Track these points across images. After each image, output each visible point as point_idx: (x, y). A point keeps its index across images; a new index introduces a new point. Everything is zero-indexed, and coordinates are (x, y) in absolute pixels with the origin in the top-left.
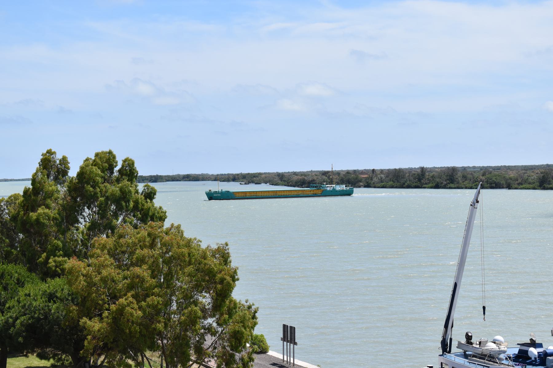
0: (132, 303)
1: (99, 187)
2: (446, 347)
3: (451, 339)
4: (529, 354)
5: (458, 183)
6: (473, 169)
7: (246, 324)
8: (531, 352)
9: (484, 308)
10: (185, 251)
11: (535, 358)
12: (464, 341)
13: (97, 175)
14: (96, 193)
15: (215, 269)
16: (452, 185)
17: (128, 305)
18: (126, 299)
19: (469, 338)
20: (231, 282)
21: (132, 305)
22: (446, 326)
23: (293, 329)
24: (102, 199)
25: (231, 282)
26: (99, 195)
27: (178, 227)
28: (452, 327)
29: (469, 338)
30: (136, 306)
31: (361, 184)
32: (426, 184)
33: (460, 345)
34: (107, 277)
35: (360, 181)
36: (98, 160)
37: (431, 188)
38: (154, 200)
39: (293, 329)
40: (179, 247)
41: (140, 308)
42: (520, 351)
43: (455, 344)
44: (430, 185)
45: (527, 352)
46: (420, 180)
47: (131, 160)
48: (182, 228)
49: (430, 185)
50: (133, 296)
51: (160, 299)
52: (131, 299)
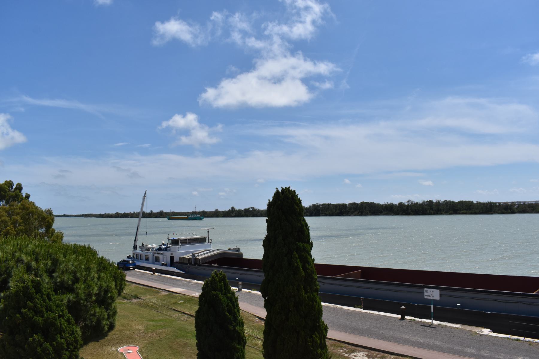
0: (12, 229)
1: (7, 193)
2: (135, 248)
3: (137, 245)
4: (162, 248)
5: (164, 216)
6: (173, 215)
7: (58, 238)
8: (162, 247)
9: (147, 233)
10: (34, 210)
11: (164, 249)
12: (141, 245)
13: (7, 188)
14: (6, 195)
15: (46, 217)
16: (161, 217)
17: (11, 229)
18: (10, 227)
19: (143, 245)
20: (52, 222)
21: (12, 230)
22: (135, 241)
23: (29, 195)
24: (8, 197)
25: (52, 222)
26: (7, 196)
27: (34, 202)
28: (137, 241)
29: (143, 245)
30: (14, 230)
31: (129, 217)
32: (152, 216)
33: (140, 247)
34: (3, 220)
35: (129, 216)
36: (6, 183)
37: (154, 218)
38: (29, 199)
39: (29, 195)
40: (32, 208)
41: (15, 231)
42: (159, 247)
43: (138, 247)
44: (154, 217)
45: (161, 247)
46: (150, 215)
47: (20, 184)
48: (35, 203)
49: (154, 217)
50: (13, 226)
51: (24, 227)
52: (12, 227)
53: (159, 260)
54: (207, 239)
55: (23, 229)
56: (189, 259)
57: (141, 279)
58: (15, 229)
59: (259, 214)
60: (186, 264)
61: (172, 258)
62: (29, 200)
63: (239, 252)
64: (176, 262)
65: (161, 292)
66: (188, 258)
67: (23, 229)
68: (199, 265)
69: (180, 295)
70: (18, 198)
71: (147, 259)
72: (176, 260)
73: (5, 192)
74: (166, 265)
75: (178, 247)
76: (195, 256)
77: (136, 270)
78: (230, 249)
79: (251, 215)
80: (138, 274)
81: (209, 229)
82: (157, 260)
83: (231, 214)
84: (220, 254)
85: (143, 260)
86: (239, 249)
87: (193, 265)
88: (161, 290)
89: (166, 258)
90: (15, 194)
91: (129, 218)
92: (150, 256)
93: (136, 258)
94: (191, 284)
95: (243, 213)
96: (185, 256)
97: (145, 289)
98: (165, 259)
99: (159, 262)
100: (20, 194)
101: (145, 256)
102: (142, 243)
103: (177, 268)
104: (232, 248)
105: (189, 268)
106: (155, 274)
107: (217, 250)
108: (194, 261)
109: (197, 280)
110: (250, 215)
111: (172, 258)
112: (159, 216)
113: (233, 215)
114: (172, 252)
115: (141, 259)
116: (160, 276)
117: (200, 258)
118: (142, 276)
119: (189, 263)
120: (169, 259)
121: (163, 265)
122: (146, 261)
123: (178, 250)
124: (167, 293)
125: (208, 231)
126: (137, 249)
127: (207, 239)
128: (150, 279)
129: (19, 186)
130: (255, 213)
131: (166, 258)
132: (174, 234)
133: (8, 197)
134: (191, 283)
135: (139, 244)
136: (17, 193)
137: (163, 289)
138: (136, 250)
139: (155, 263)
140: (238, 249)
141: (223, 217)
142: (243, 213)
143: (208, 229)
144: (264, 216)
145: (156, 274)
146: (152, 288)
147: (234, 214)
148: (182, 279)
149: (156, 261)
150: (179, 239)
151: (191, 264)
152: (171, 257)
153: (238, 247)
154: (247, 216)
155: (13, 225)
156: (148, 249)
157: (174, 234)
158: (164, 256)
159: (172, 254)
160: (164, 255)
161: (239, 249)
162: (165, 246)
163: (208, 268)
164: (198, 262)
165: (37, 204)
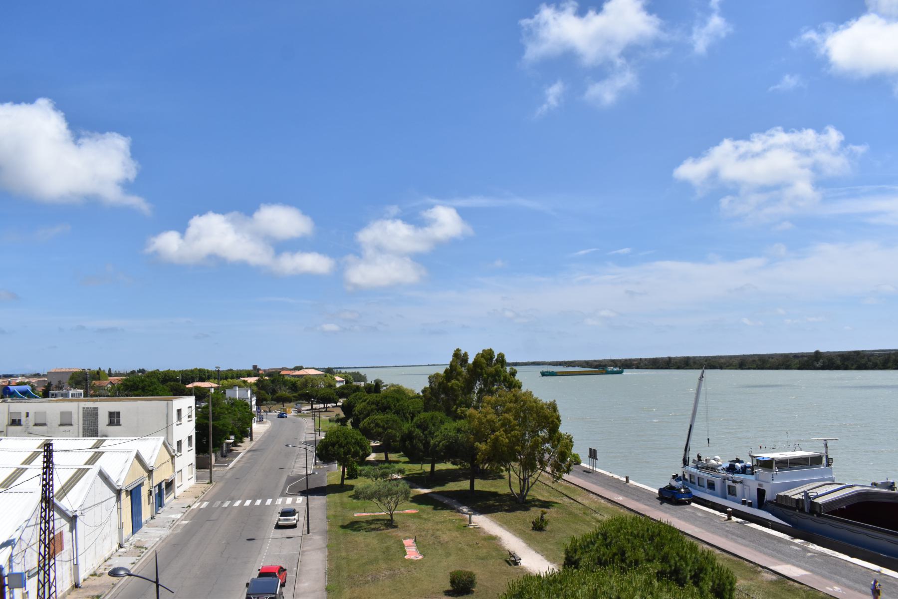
1: (485, 370)
2: (685, 462)
3: (689, 458)
5: (691, 366)
8: (737, 466)
12: (696, 459)
16: (687, 367)
17: (501, 436)
19: (699, 457)
27: (531, 392)
28: (689, 450)
29: (699, 457)
30: (505, 436)
31: (634, 367)
33: (694, 461)
35: (633, 365)
38: (515, 377)
41: (507, 438)
42: (730, 465)
44: (675, 367)
46: (668, 364)
49: (675, 367)
50: (503, 431)
51: (519, 432)
52: (502, 432)
53: (736, 492)
54: (824, 459)
55: (518, 434)
56: (798, 501)
57: (709, 531)
58: (507, 435)
59: (871, 363)
60: (794, 509)
61: (761, 493)
62: (515, 379)
63: (894, 490)
64: (770, 502)
65: (760, 572)
66: (796, 497)
67: (518, 434)
68: (819, 515)
69: (801, 586)
70: (499, 376)
71: (711, 486)
72: (768, 496)
73: (482, 369)
74: (750, 505)
75: (773, 475)
76: (809, 497)
77: (693, 504)
78: (875, 485)
79: (855, 366)
80: (700, 517)
81: (828, 441)
82: (731, 492)
83: (815, 363)
84: (860, 495)
85: (704, 487)
86: (893, 483)
87: (807, 513)
88: (760, 569)
89: (749, 489)
90: (495, 370)
91: (633, 368)
92: (718, 483)
93: (689, 479)
94: (809, 554)
95: (839, 362)
96: (790, 493)
97: (729, 560)
98: (746, 492)
99: (735, 495)
100: (502, 370)
101: (708, 480)
102: (698, 455)
103: (774, 514)
104: (879, 482)
105: (798, 518)
106: (731, 519)
107: (852, 486)
108: (808, 506)
109: (818, 545)
110: (852, 365)
111: (761, 493)
112: (683, 366)
113: (818, 365)
114: (761, 483)
115: (699, 485)
116: (740, 526)
117: (820, 501)
118: (708, 522)
119: (798, 507)
120: (755, 494)
121: (744, 503)
122: (710, 491)
123: (773, 480)
124: (774, 577)
125: (826, 444)
126: (689, 463)
127: (824, 459)
128: (728, 534)
129: (501, 357)
130: (863, 361)
131: (749, 489)
132: (761, 447)
133: (485, 375)
134: (809, 552)
135: (693, 456)
136: (498, 370)
137: (764, 565)
138: (688, 465)
139: (728, 496)
140: (890, 485)
141: (799, 369)
142: (839, 362)
143: (825, 440)
144: (882, 367)
145: (734, 519)
146: (741, 560)
147: (820, 364)
148: (786, 537)
149: (729, 493)
150: (773, 459)
151: (802, 510)
152: (758, 490)
153: (890, 480)
154: (846, 368)
155: (504, 429)
156: (713, 469)
157: (761, 447)
158: (745, 487)
159: (760, 485)
160: (744, 485)
161: (893, 483)
162: (742, 464)
163: (843, 525)
164: (818, 510)
165: (536, 395)
